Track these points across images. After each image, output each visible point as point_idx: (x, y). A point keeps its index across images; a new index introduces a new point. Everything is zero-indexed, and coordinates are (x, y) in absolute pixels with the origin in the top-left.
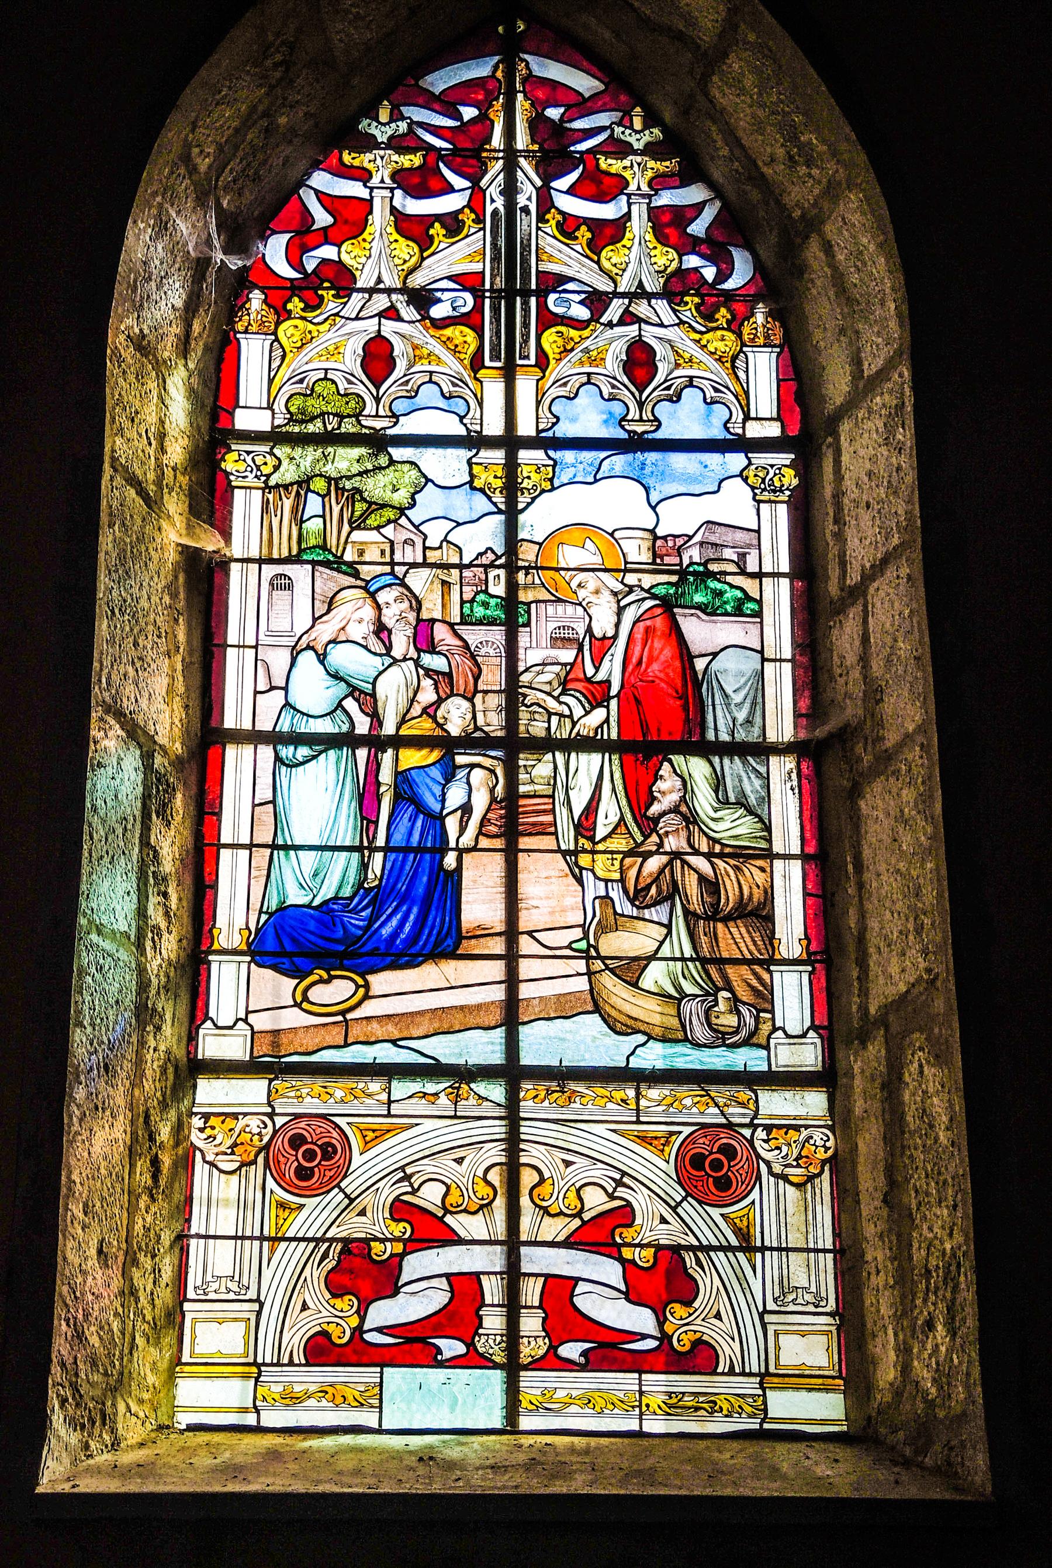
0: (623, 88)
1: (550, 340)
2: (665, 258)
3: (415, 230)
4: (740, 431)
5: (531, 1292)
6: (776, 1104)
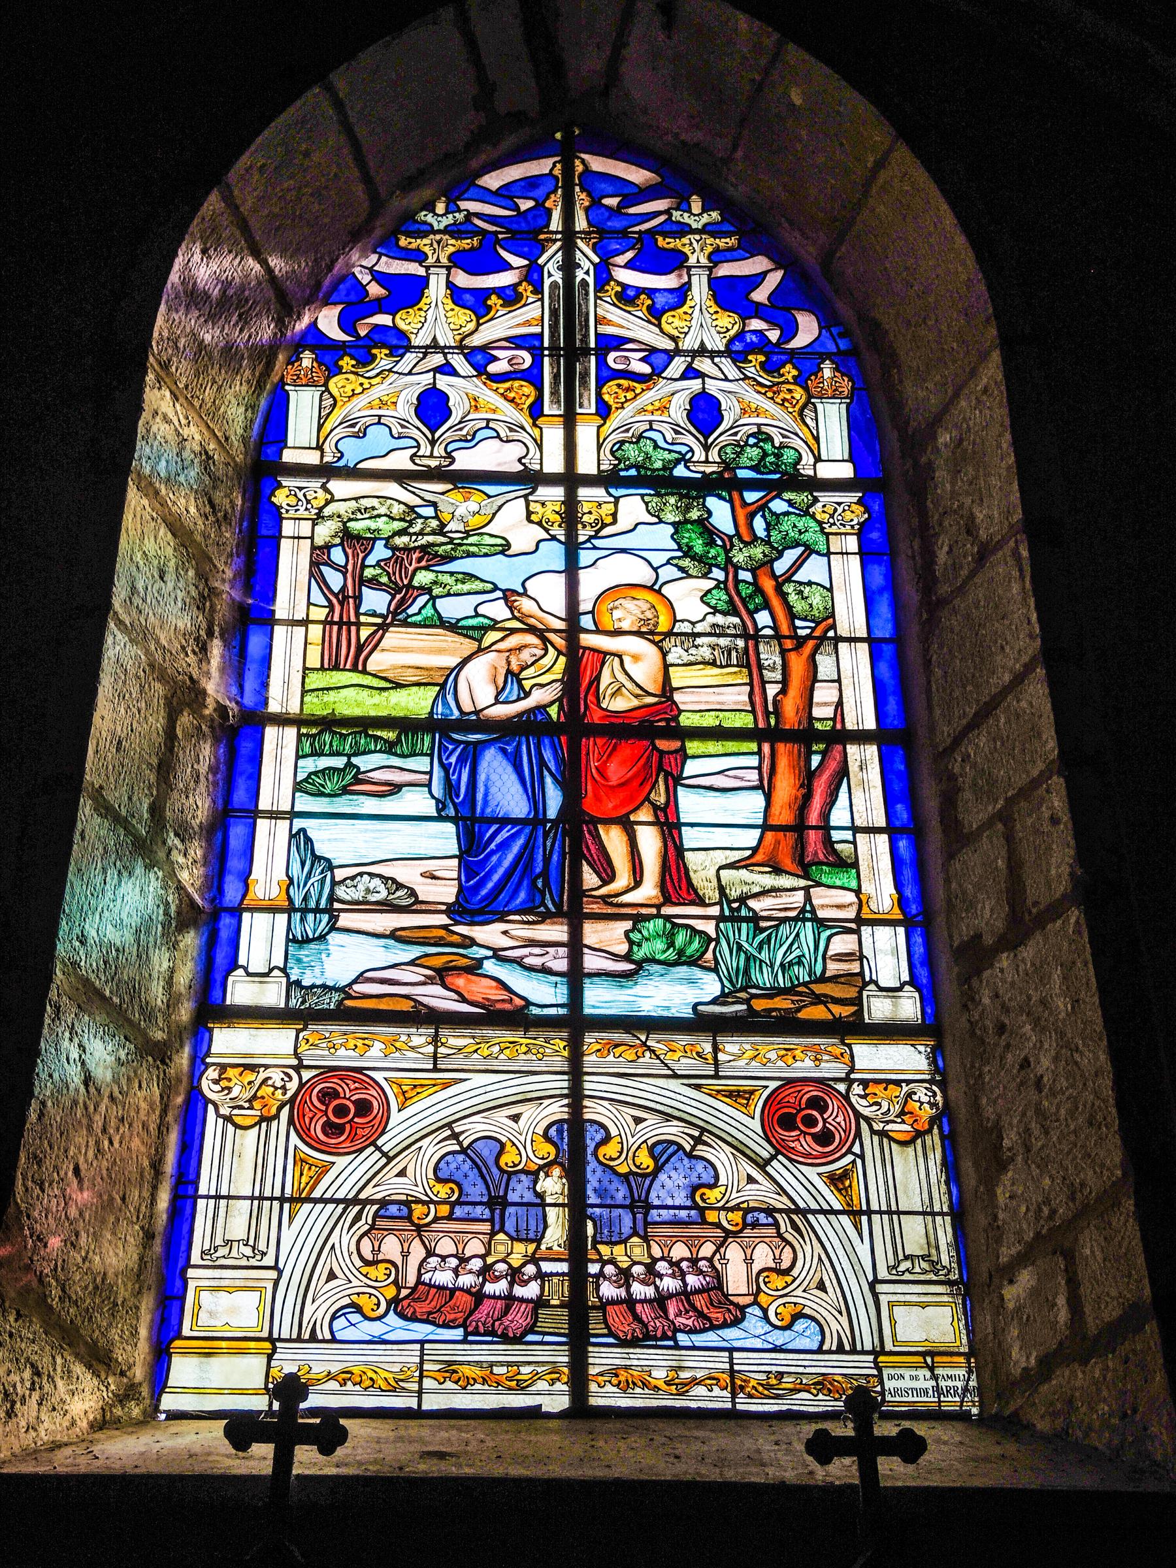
0: (676, 182)
1: (610, 391)
2: (728, 321)
4: (811, 473)
6: (871, 1057)
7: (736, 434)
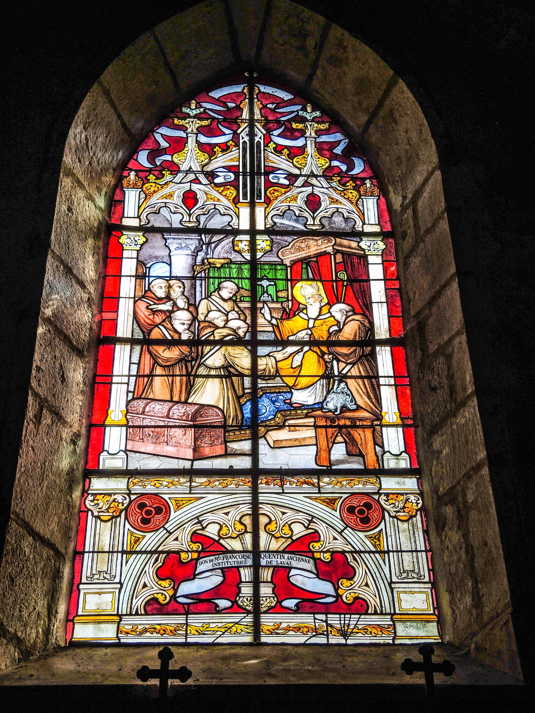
2: (324, 162)
3: (209, 150)
4: (361, 229)
5: (266, 574)
6: (389, 484)
7: (327, 212)
